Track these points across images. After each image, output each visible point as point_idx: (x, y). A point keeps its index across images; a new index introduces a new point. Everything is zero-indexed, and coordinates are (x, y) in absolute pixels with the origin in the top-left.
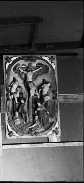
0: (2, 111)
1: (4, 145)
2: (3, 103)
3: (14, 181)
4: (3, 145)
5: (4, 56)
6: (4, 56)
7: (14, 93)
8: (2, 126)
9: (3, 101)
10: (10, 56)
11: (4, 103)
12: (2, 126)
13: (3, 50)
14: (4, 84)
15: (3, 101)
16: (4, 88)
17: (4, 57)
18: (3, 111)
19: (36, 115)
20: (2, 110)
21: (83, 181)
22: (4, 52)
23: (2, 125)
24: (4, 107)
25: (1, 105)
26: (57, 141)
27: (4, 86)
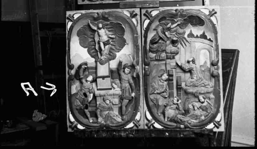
0: (156, 6)
1: (205, 3)
2: (146, 5)
3: (254, 35)
4: (203, 4)
5: (79, 4)
6: (79, 4)
7: (124, 70)
8: (178, 5)
9: (142, 4)
10: (68, 124)
11: (145, 4)
12: (178, 5)
13: (71, 5)
14: (119, 3)
15: (142, 4)
16: (124, 3)
17: (69, 130)
18: (157, 4)
19: (150, 129)
20: (154, 6)
21: (252, 143)
22: (73, 3)
23: (177, 6)
24: (150, 4)
25: (147, 7)
26: (196, 43)
27: (120, 3)
